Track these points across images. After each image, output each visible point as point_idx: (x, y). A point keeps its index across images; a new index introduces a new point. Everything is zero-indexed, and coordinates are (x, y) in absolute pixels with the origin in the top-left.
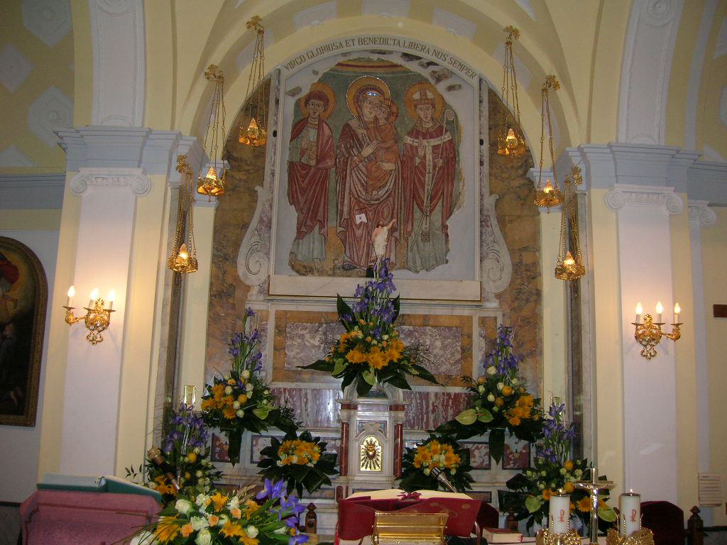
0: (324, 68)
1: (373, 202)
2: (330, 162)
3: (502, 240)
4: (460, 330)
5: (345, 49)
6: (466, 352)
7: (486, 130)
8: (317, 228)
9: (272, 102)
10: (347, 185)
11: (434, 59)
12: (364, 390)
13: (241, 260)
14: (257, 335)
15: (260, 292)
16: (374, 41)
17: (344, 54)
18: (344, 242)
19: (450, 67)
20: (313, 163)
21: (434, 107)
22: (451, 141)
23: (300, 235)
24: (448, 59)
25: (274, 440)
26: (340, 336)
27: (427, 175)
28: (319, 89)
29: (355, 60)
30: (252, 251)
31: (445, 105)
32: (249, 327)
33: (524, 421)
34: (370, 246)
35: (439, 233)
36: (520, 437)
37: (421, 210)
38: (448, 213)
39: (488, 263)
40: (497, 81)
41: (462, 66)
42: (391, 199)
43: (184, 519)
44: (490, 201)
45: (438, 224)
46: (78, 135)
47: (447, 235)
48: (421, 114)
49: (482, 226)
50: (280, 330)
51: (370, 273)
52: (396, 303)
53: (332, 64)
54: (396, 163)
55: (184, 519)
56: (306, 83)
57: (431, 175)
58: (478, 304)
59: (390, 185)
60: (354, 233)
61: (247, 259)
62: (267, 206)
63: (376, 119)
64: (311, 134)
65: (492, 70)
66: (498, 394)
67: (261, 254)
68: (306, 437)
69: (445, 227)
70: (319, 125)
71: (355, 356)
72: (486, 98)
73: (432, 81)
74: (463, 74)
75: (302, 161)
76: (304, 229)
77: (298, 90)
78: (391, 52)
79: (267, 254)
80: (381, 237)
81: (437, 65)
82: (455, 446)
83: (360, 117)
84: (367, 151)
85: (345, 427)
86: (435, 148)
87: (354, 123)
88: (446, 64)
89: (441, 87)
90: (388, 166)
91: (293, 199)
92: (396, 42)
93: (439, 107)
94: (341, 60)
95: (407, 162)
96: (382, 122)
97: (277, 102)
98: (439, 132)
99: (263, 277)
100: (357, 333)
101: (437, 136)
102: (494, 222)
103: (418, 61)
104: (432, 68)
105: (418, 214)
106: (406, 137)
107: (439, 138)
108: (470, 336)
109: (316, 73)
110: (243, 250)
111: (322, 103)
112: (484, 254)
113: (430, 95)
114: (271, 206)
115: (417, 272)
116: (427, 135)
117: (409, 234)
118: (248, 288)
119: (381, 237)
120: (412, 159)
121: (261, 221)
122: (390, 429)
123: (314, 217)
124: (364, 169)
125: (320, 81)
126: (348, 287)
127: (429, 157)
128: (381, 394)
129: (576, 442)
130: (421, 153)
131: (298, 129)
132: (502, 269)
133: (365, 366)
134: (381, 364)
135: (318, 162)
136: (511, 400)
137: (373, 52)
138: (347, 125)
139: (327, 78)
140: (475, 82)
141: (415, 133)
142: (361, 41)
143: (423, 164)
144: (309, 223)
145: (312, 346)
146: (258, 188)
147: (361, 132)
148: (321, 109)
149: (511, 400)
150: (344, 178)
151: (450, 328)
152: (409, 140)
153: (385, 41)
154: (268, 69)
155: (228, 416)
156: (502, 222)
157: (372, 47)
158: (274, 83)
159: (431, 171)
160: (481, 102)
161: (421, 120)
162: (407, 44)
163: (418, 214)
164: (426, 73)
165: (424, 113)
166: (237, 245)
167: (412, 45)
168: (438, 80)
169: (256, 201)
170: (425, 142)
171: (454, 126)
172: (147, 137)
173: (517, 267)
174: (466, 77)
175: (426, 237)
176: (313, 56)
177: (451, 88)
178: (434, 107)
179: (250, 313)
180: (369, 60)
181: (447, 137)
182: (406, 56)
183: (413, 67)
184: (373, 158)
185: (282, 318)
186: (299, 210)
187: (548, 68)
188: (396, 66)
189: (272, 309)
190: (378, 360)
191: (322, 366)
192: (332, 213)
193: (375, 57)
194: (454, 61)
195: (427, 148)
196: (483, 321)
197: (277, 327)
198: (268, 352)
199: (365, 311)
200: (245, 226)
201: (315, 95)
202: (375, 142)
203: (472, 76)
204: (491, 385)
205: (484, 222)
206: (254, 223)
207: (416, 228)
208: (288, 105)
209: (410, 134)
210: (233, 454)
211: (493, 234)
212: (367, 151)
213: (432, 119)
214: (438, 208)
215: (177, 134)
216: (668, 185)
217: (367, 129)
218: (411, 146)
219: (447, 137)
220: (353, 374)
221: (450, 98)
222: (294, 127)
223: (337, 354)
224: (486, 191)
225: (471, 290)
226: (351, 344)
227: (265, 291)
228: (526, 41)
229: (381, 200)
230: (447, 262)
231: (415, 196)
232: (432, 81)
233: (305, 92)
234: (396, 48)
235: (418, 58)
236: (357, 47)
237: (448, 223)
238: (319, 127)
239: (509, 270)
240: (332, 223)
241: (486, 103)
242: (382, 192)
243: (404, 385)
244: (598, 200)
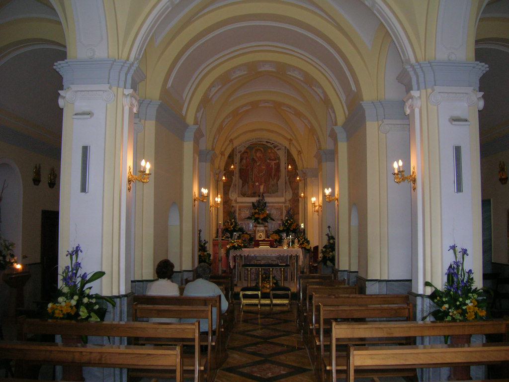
4: (280, 209)
6: (282, 214)
11: (273, 142)
12: (259, 223)
13: (230, 194)
14: (235, 212)
16: (259, 138)
25: (240, 235)
26: (253, 211)
32: (232, 210)
33: (294, 229)
34: (259, 190)
36: (293, 232)
38: (278, 180)
39: (287, 193)
40: (288, 147)
41: (281, 144)
43: (233, 243)
44: (287, 178)
46: (67, 64)
50: (239, 210)
51: (259, 196)
52: (265, 203)
55: (233, 243)
56: (243, 150)
58: (284, 203)
59: (264, 172)
65: (286, 144)
66: (288, 223)
68: (246, 233)
69: (277, 183)
71: (256, 216)
72: (286, 152)
79: (236, 192)
80: (262, 187)
82: (279, 235)
83: (256, 156)
85: (255, 231)
87: (255, 157)
89: (276, 149)
90: (264, 167)
91: (241, 178)
94: (251, 143)
95: (268, 165)
96: (261, 157)
98: (275, 160)
99: (235, 198)
100: (257, 211)
102: (288, 183)
105: (271, 180)
108: (282, 210)
110: (230, 192)
116: (273, 160)
118: (232, 200)
119: (262, 187)
120: (269, 165)
122: (264, 231)
126: (254, 200)
127: (273, 166)
128: (262, 224)
129: (304, 234)
131: (241, 159)
133: (258, 218)
134: (262, 217)
136: (290, 225)
138: (253, 158)
139: (247, 148)
141: (270, 159)
143: (272, 167)
145: (246, 213)
149: (290, 225)
151: (278, 208)
152: (268, 161)
154: (234, 147)
155: (229, 229)
156: (290, 182)
158: (235, 150)
163: (271, 180)
164: (272, 146)
165: (272, 155)
166: (229, 191)
167: (269, 139)
168: (275, 147)
171: (279, 159)
172: (112, 64)
173: (293, 193)
177: (278, 149)
179: (233, 206)
183: (269, 145)
184: (259, 165)
185: (239, 207)
186: (242, 180)
187: (299, 149)
189: (238, 205)
190: (262, 217)
191: (249, 218)
195: (273, 163)
196: (285, 206)
197: (239, 209)
198: (237, 215)
199: (258, 207)
200: (230, 186)
201: (245, 152)
204: (287, 221)
205: (286, 183)
206: (232, 185)
208: (239, 156)
210: (231, 237)
214: (276, 179)
215: (130, 64)
216: (483, 62)
220: (256, 220)
221: (277, 152)
222: (240, 159)
223: (253, 215)
224: (286, 176)
225: (282, 199)
226: (255, 213)
227: (236, 201)
228: (294, 142)
233: (243, 152)
237: (278, 182)
239: (291, 194)
241: (286, 154)
243: (267, 222)
244: (372, 128)
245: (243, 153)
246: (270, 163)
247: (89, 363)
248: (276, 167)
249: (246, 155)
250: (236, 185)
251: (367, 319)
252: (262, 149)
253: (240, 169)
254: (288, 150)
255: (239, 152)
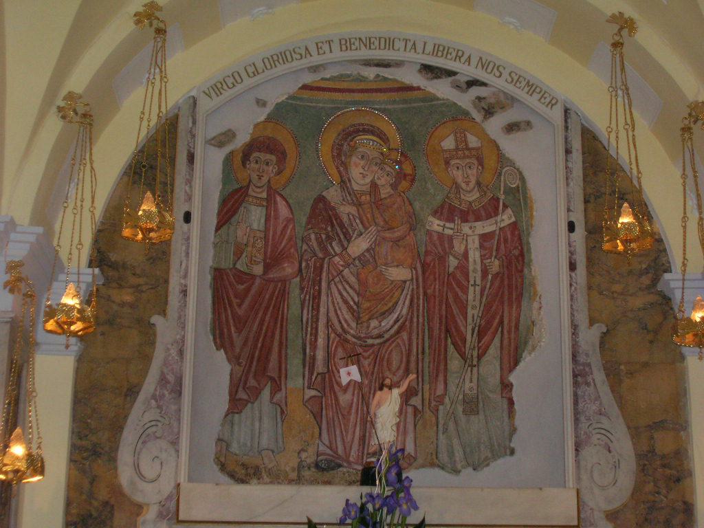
0: (277, 95)
1: (370, 341)
2: (289, 269)
3: (615, 411)
5: (316, 59)
7: (579, 205)
8: (266, 393)
9: (182, 158)
10: (323, 310)
11: (481, 75)
13: (125, 456)
15: (161, 516)
16: (368, 42)
17: (314, 69)
18: (317, 416)
19: (510, 89)
20: (258, 270)
21: (481, 163)
22: (514, 226)
23: (236, 405)
24: (505, 75)
27: (471, 289)
28: (269, 133)
29: (332, 79)
30: (145, 438)
31: (501, 158)
35: (496, 397)
37: (463, 355)
38: (512, 360)
39: (592, 454)
40: (599, 120)
41: (532, 87)
42: (405, 335)
44: (590, 336)
45: (494, 381)
47: (511, 402)
48: (458, 175)
49: (576, 384)
51: (368, 477)
53: (292, 87)
54: (413, 267)
57: (478, 289)
59: (402, 309)
60: (337, 399)
61: (136, 453)
62: (174, 352)
63: (374, 186)
64: (254, 217)
67: (163, 444)
69: (506, 387)
70: (269, 199)
72: (577, 144)
73: (477, 116)
74: (533, 101)
75: (238, 266)
76: (242, 395)
77: (229, 135)
78: (399, 64)
79: (175, 443)
80: (387, 408)
81: (484, 84)
83: (344, 183)
84: (359, 246)
86: (485, 237)
87: (333, 195)
88: (501, 84)
89: (494, 126)
90: (398, 274)
92: (410, 45)
93: (491, 162)
94: (309, 79)
96: (385, 192)
97: (191, 158)
98: (492, 209)
99: (167, 487)
101: (489, 217)
102: (599, 376)
103: (450, 79)
104: (476, 91)
105: (455, 363)
106: (431, 219)
107: (492, 220)
109: (261, 103)
110: (129, 436)
111: (273, 158)
112: (583, 437)
113: (473, 141)
114: (181, 353)
115: (457, 472)
117: (440, 400)
118: (139, 508)
119: (387, 408)
120: (442, 259)
121: (163, 380)
123: (262, 372)
124: (352, 280)
125: (269, 119)
127: (474, 255)
130: (459, 247)
131: (230, 207)
132: (616, 466)
135: (267, 268)
137: (368, 63)
138: (321, 199)
140: (557, 115)
141: (447, 211)
142: (346, 44)
143: (463, 269)
144: (252, 382)
146: (156, 319)
147: (346, 211)
148: (271, 170)
150: (317, 297)
152: (436, 224)
153: (389, 43)
154: (176, 95)
156: (612, 372)
157: (364, 53)
158: (184, 124)
159: (479, 282)
160: (568, 152)
161: (458, 187)
162: (429, 48)
163: (455, 363)
164: (465, 100)
165: (464, 175)
166: (117, 427)
167: (439, 49)
168: (489, 112)
169: (153, 344)
170: (466, 228)
171: (519, 197)
173: (647, 460)
174: (542, 109)
175: (472, 406)
176: (256, 73)
177: (511, 128)
178: (481, 163)
180: (361, 79)
181: (506, 218)
182: (430, 71)
183: (442, 89)
184: (369, 259)
186: (233, 359)
188: (410, 88)
192: (295, 364)
193: (370, 73)
194: (517, 78)
202: (373, 229)
203: (552, 104)
205: (580, 376)
206: (150, 385)
207: (452, 388)
208: (211, 164)
209: (437, 213)
211: (598, 398)
212: (359, 246)
213: (479, 184)
214: (493, 351)
217: (359, 205)
218: (441, 236)
219: (506, 218)
221: (511, 146)
222: (224, 202)
224: (582, 318)
229: (387, 336)
230: (512, 452)
231: (450, 329)
232: (477, 116)
233: (243, 139)
234: (410, 56)
235: (451, 73)
236: (337, 54)
238: (269, 203)
240: (295, 381)
241: (577, 156)
242: (387, 322)
245: (247, 152)
246: (446, 242)
247: (700, 280)
248: (495, 265)
249: (263, 169)
250: (178, 392)
251: (178, 482)
252: (391, 130)
253: (219, 275)
254: (589, 136)
255: (221, 140)
